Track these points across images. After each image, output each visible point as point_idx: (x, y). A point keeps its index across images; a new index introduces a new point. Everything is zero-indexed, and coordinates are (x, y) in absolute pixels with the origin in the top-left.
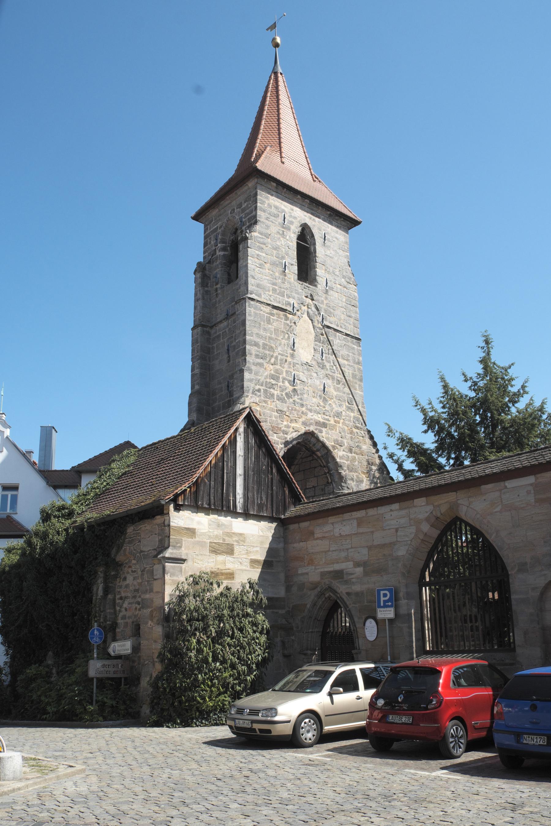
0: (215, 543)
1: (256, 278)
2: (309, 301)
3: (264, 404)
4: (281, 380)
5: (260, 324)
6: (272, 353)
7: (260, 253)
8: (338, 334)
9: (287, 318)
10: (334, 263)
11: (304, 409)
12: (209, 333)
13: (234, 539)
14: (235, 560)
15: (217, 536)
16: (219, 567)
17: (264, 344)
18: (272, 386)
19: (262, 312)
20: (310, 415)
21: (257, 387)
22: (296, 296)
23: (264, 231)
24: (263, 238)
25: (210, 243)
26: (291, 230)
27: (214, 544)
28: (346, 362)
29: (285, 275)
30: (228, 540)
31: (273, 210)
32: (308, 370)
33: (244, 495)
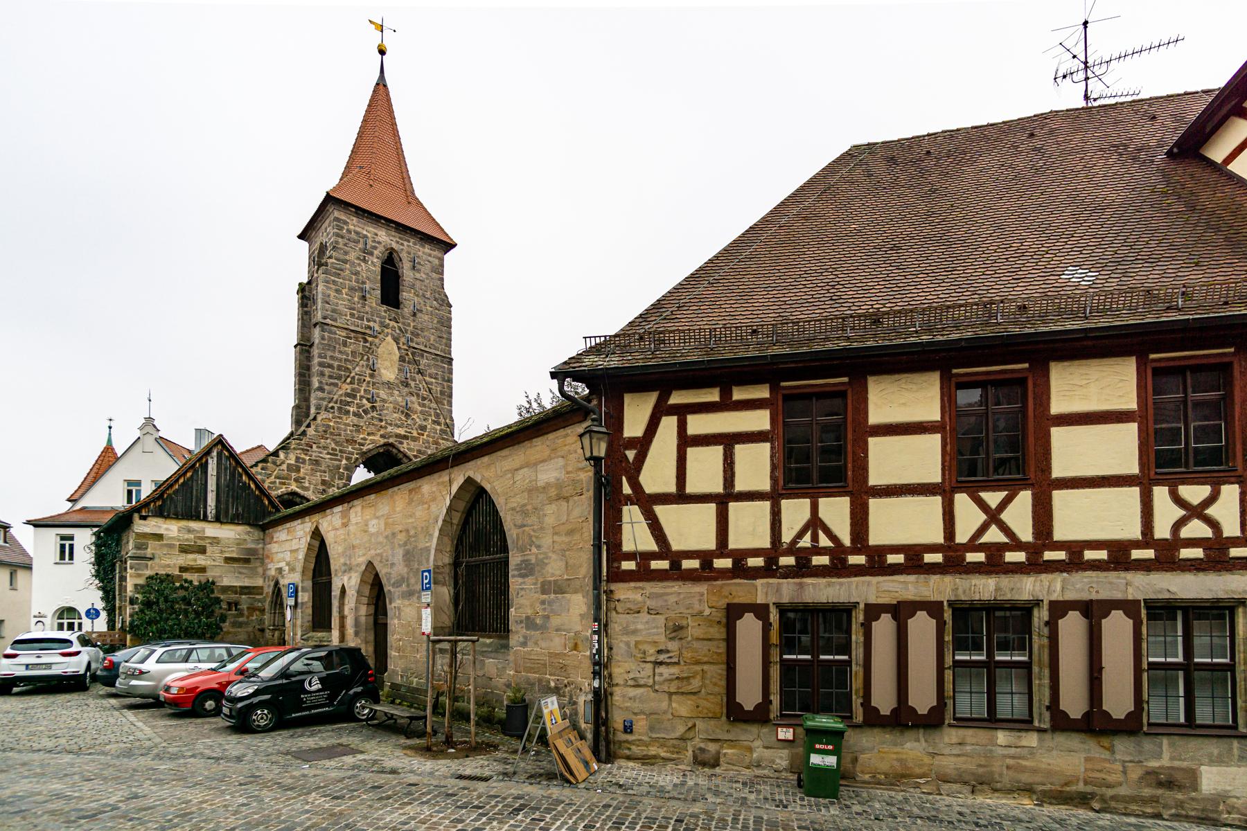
2: (392, 323)
5: (335, 347)
6: (348, 374)
7: (336, 279)
8: (425, 354)
9: (366, 341)
10: (425, 286)
11: (383, 424)
15: (187, 540)
17: (339, 366)
18: (348, 404)
19: (337, 336)
20: (389, 429)
21: (330, 405)
22: (377, 319)
23: (342, 257)
28: (434, 380)
29: (366, 300)
30: (200, 543)
31: (353, 235)
32: (389, 388)
33: (217, 507)
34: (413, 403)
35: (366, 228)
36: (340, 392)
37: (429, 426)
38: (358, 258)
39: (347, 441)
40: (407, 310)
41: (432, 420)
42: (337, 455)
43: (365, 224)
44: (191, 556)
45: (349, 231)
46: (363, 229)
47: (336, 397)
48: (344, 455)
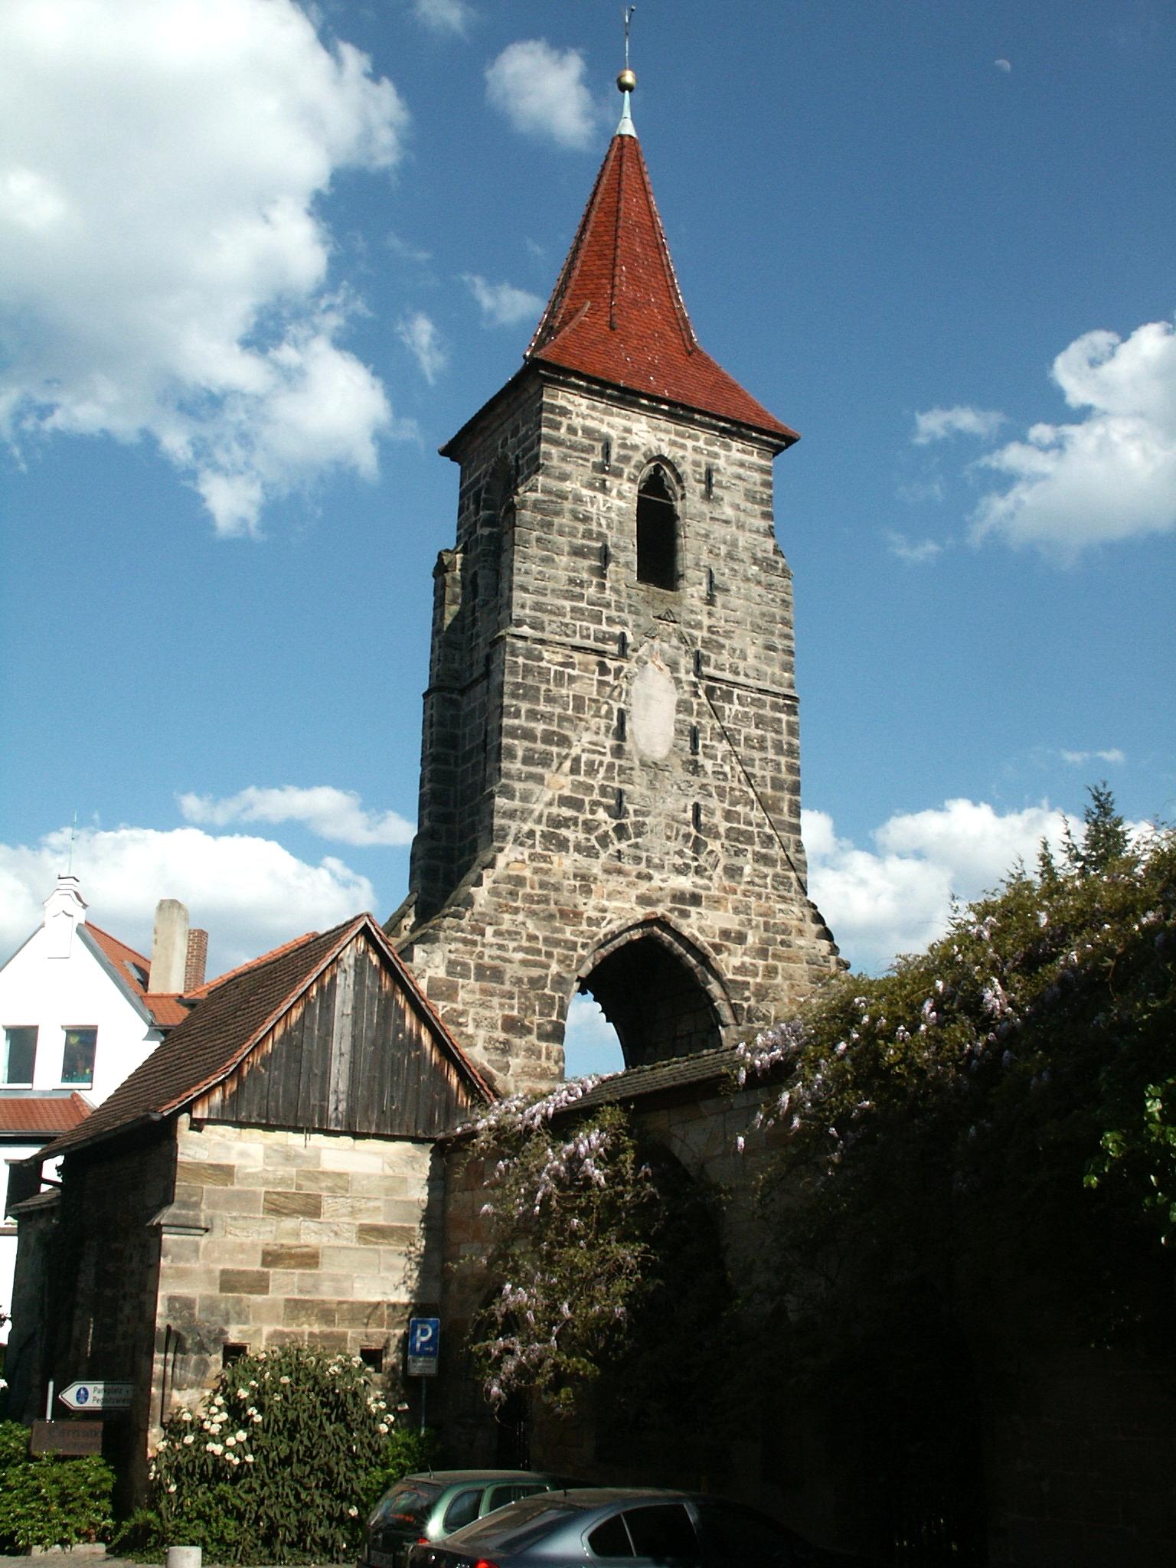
0: (278, 1193)
1: (531, 589)
3: (543, 865)
4: (587, 807)
6: (564, 752)
8: (736, 691)
9: (603, 669)
11: (643, 866)
12: (455, 704)
13: (323, 1185)
14: (324, 1227)
15: (282, 1181)
16: (284, 1242)
18: (565, 823)
19: (543, 664)
21: (526, 828)
24: (552, 502)
25: (468, 508)
26: (625, 476)
27: (275, 1197)
30: (310, 1188)
31: (580, 438)
34: (711, 813)
35: (607, 419)
36: (548, 796)
37: (747, 870)
38: (590, 486)
39: (563, 914)
40: (693, 591)
41: (755, 853)
42: (538, 952)
43: (605, 412)
44: (289, 1223)
45: (572, 430)
46: (602, 421)
47: (538, 808)
48: (556, 951)
